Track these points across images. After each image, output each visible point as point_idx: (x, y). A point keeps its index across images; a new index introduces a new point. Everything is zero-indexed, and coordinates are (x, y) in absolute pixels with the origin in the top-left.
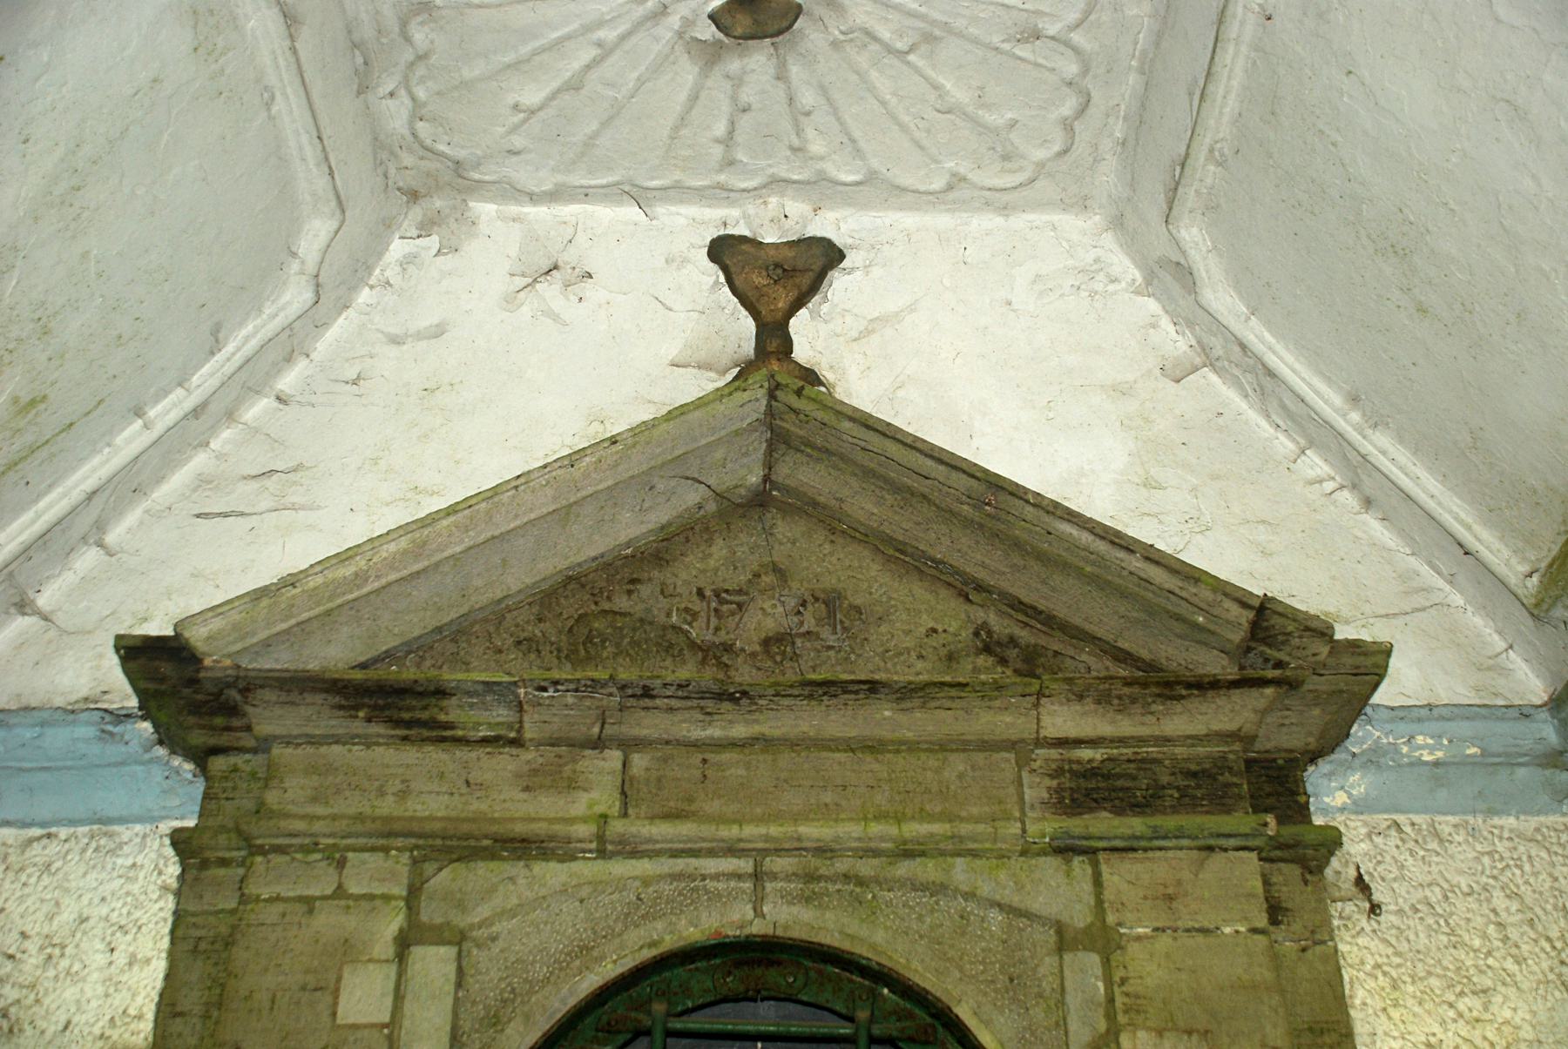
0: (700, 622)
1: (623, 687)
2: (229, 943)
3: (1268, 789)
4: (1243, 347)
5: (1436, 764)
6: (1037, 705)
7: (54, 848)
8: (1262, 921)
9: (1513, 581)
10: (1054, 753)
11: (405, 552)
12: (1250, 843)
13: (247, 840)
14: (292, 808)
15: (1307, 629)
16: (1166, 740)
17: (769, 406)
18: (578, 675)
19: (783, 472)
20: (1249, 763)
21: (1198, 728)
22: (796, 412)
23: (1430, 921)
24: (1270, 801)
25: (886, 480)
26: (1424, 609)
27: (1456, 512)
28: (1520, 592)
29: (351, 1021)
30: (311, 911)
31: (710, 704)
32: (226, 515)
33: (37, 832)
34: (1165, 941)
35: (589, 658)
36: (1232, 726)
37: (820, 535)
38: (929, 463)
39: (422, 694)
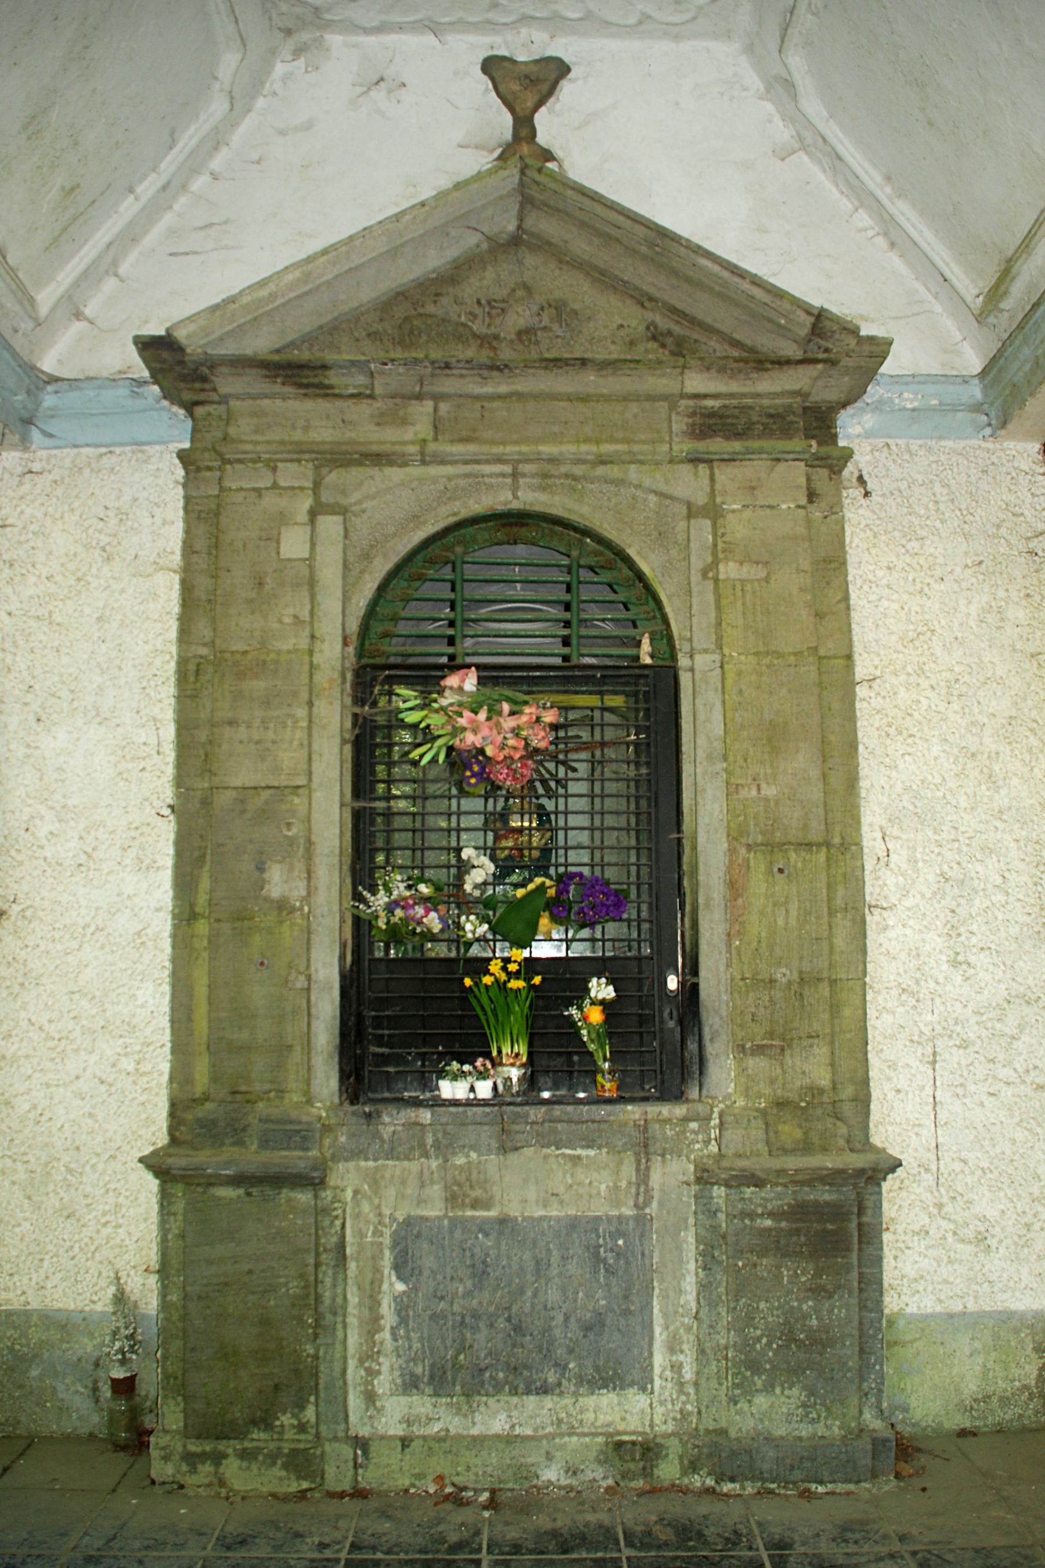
0: (479, 321)
1: (433, 363)
2: (217, 514)
3: (815, 424)
4: (824, 140)
5: (914, 410)
6: (682, 373)
7: (114, 459)
8: (803, 501)
9: (969, 299)
10: (691, 403)
11: (298, 280)
12: (801, 457)
13: (221, 456)
14: (244, 437)
15: (845, 329)
16: (758, 395)
17: (521, 180)
18: (406, 355)
19: (529, 223)
20: (805, 409)
21: (777, 388)
22: (537, 183)
23: (899, 500)
24: (815, 432)
25: (595, 229)
26: (918, 314)
27: (941, 254)
28: (972, 306)
29: (288, 556)
30: (260, 496)
31: (485, 373)
32: (187, 254)
33: (104, 450)
34: (748, 513)
35: (412, 344)
36: (796, 387)
37: (553, 265)
38: (621, 218)
39: (314, 368)
